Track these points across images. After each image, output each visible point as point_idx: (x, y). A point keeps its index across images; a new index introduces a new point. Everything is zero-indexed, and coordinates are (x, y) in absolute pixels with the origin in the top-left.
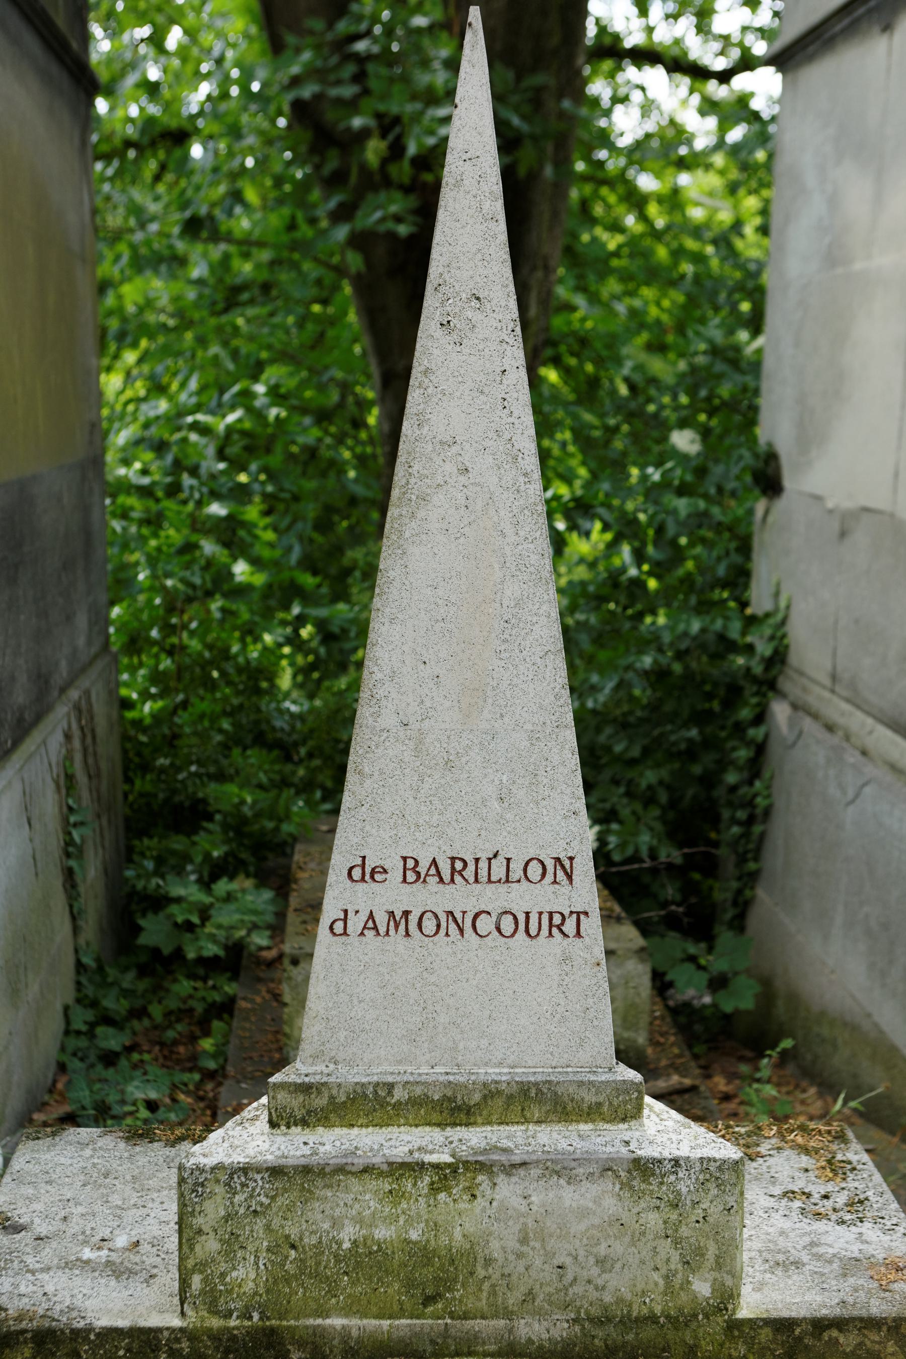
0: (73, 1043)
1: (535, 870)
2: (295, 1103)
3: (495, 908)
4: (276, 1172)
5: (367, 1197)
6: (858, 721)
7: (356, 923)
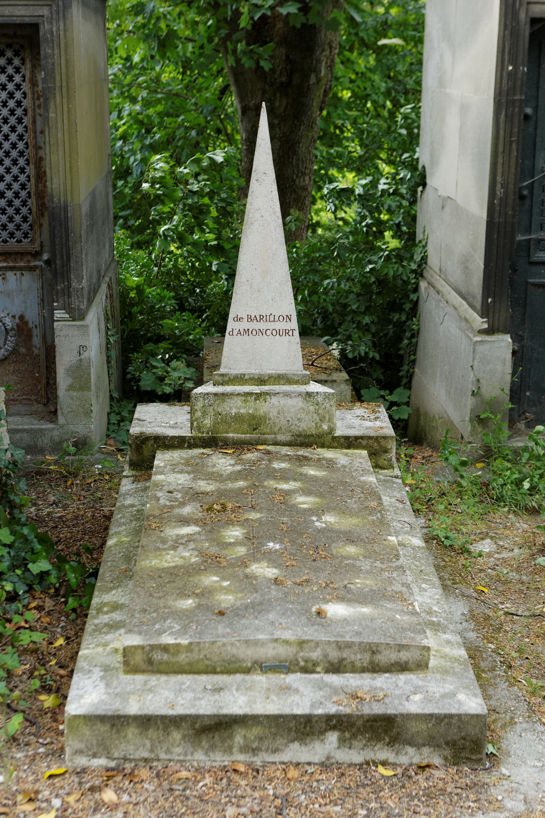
0: (112, 428)
2: (220, 379)
3: (271, 328)
4: (216, 394)
5: (239, 401)
6: (446, 289)
7: (235, 332)
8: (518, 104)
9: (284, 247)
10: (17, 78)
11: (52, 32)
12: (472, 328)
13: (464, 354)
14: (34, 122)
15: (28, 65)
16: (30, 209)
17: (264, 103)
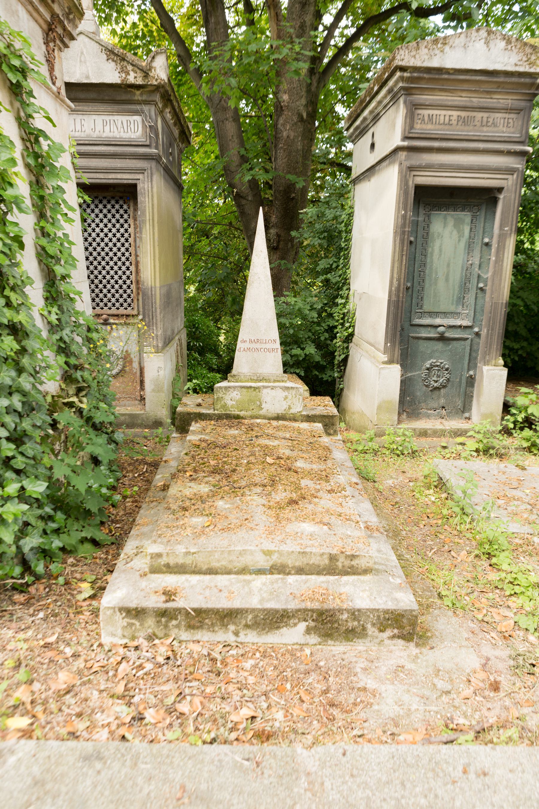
9: (272, 299)
10: (126, 216)
14: (135, 241)
15: (132, 208)
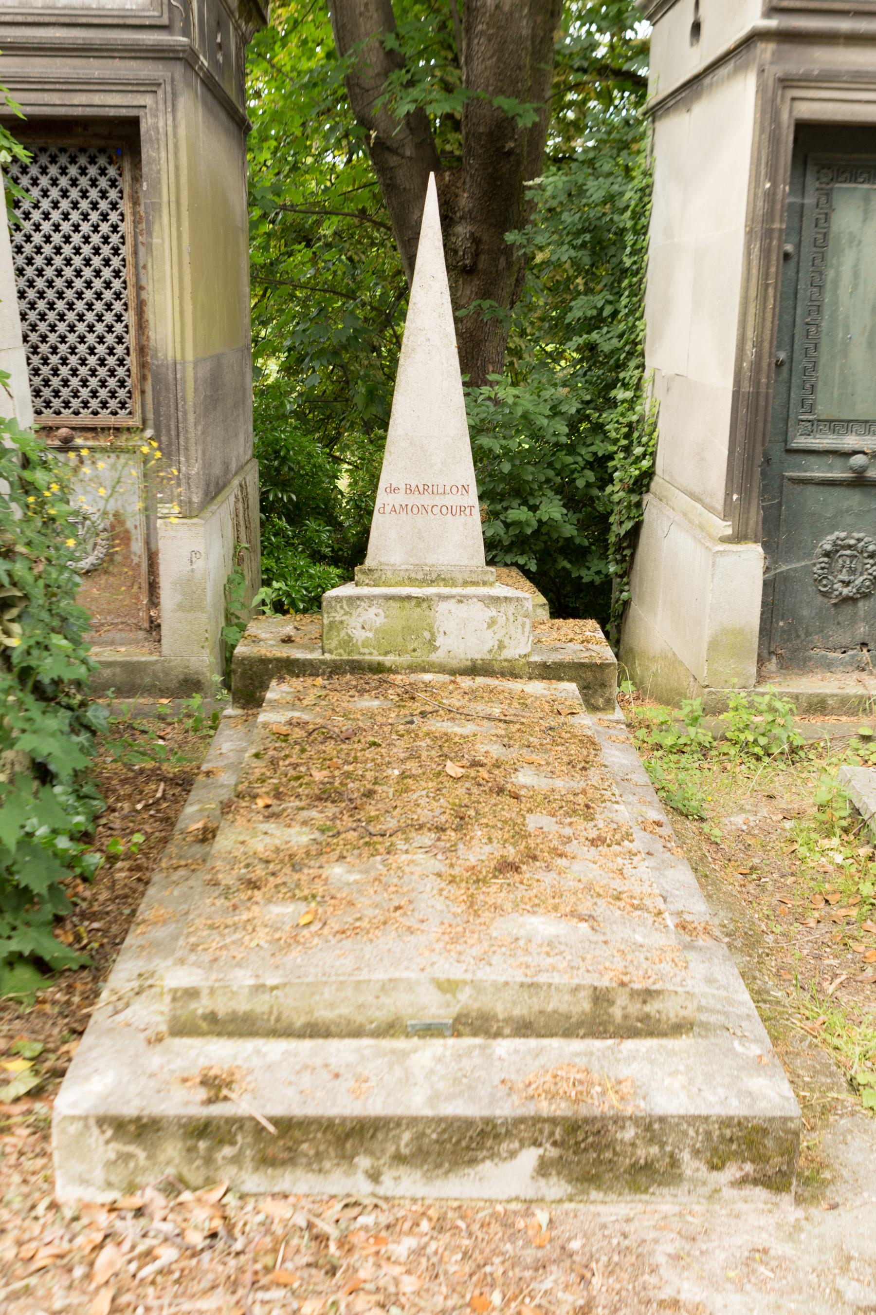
1: (454, 490)
7: (388, 509)
8: (776, 234)
10: (113, 194)
11: (157, 128)
12: (710, 536)
13: (699, 573)
14: (135, 253)
15: (127, 176)
16: (128, 370)
17: (432, 175)
